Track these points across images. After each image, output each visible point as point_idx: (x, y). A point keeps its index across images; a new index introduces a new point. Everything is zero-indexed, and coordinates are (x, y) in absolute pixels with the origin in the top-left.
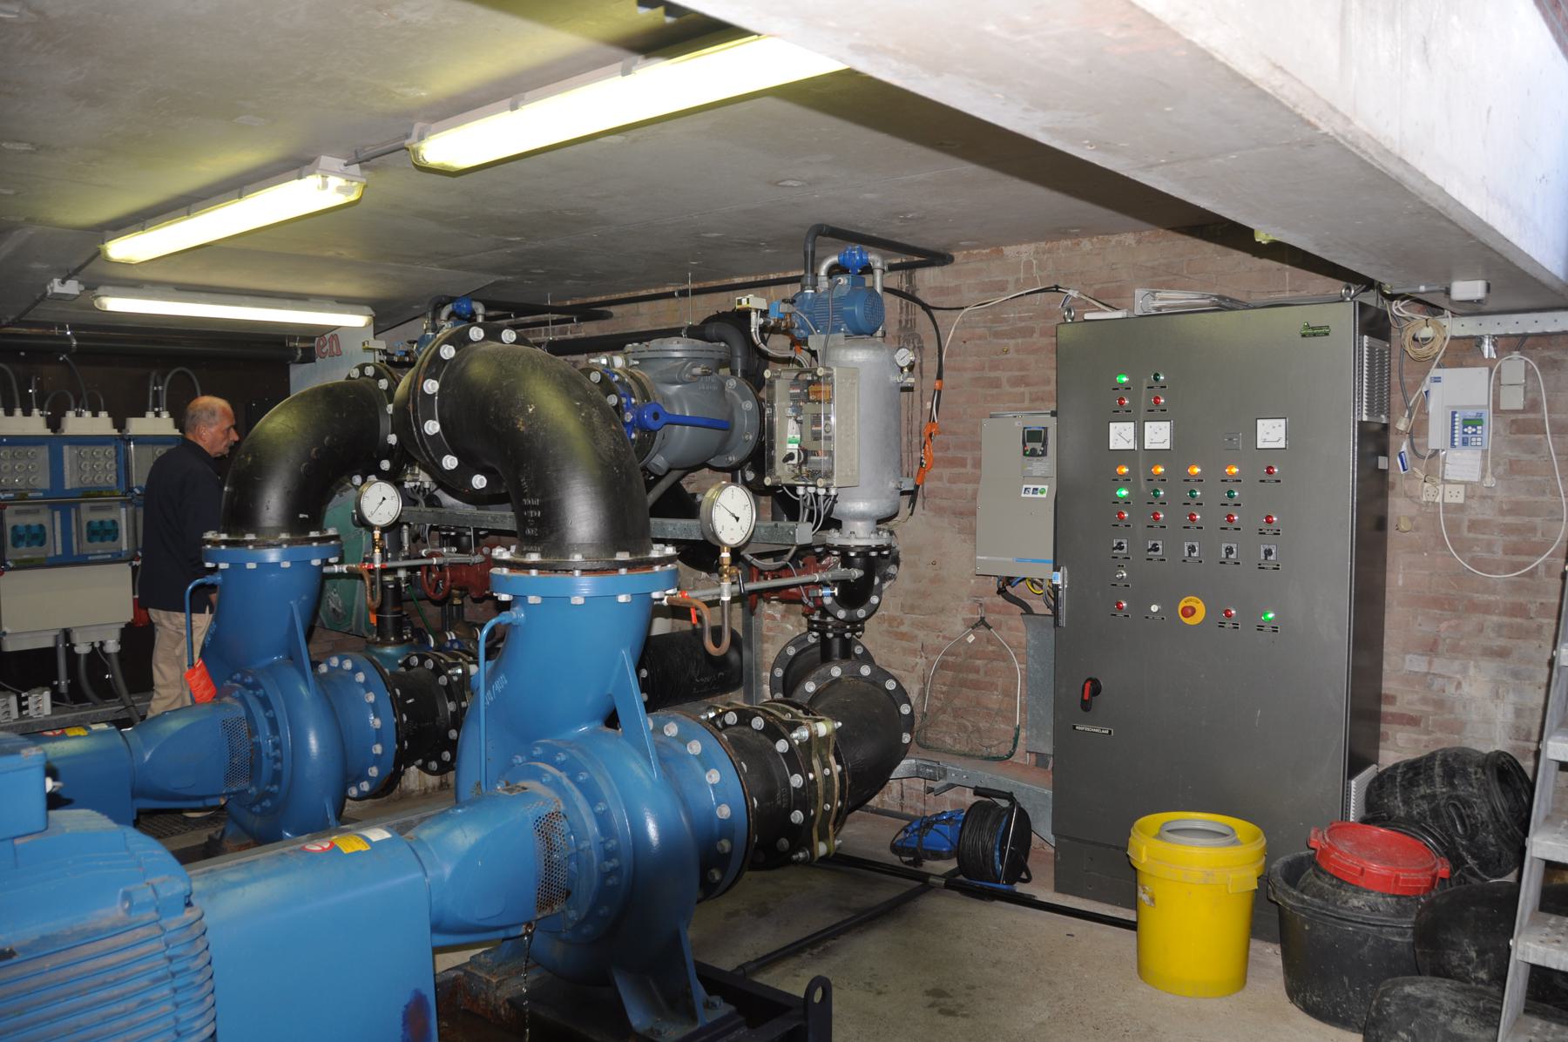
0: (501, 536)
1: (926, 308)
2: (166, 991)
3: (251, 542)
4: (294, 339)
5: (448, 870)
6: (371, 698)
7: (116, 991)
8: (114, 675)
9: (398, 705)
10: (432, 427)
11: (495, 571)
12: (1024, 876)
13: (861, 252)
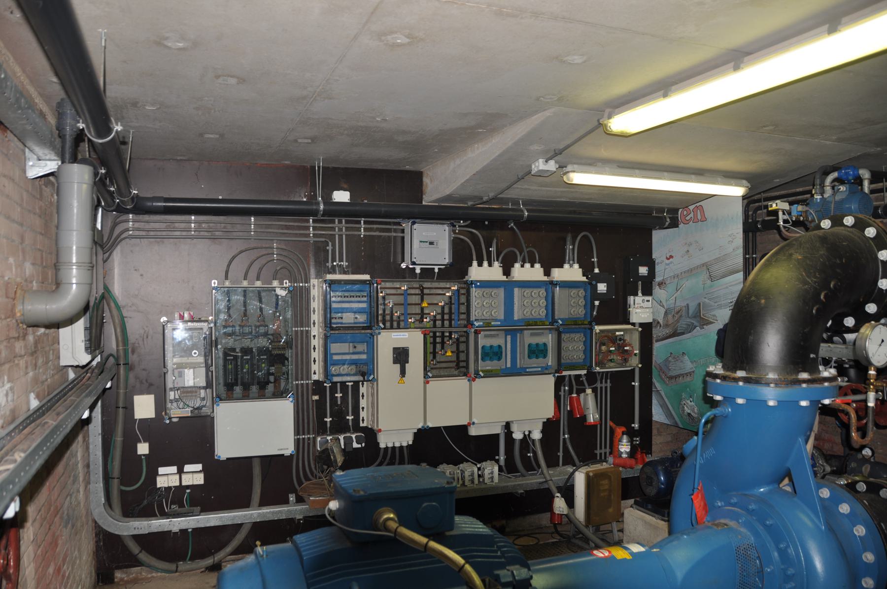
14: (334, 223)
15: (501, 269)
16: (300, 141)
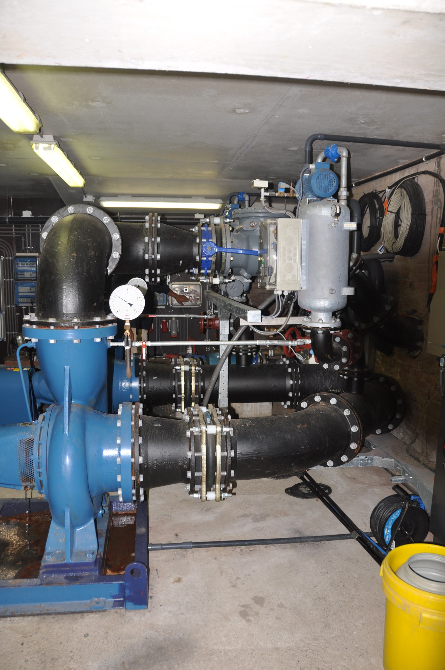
14: (25, 227)
16: (238, 111)
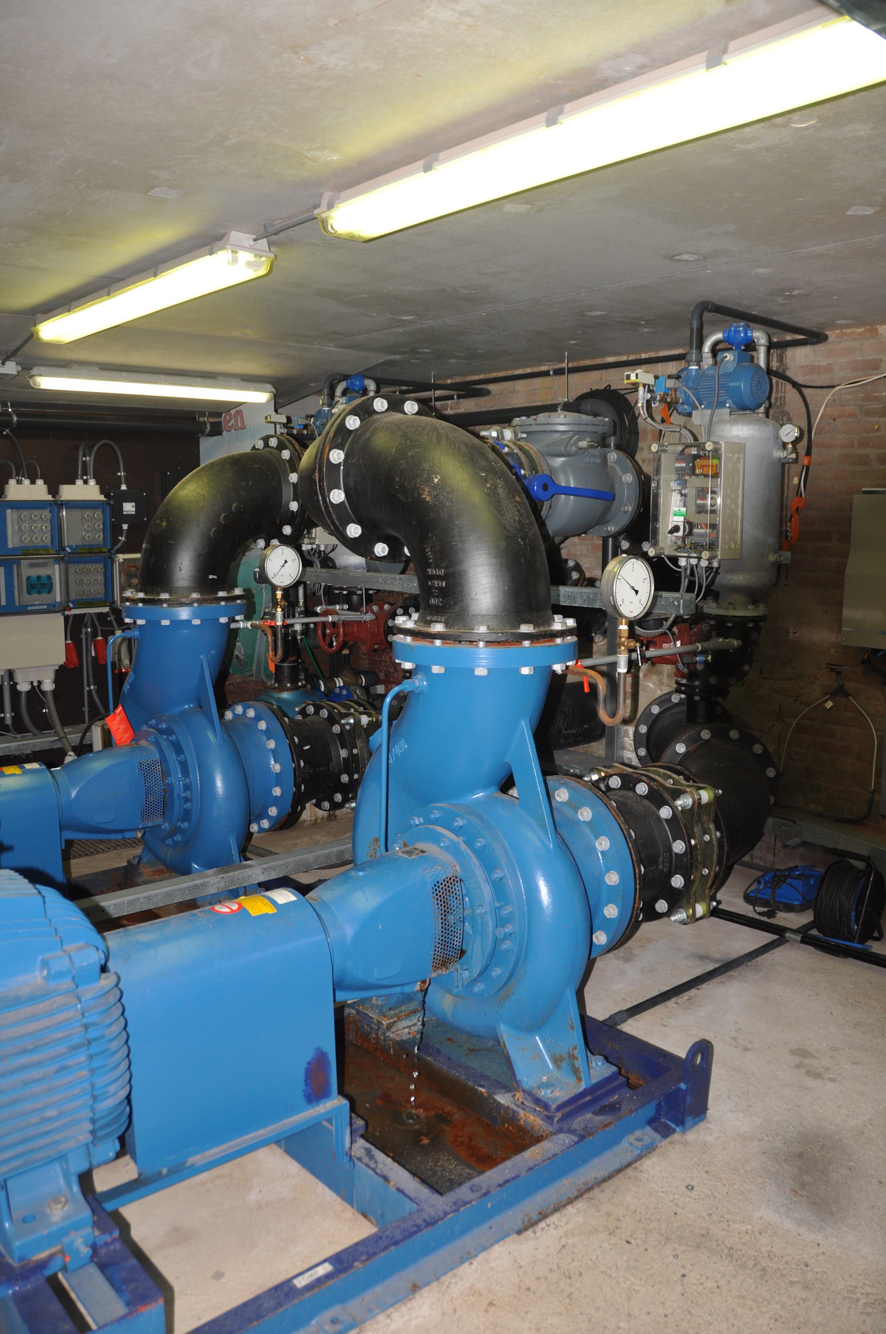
0: (409, 604)
1: (796, 386)
2: (83, 1058)
3: (165, 601)
4: (202, 414)
5: (349, 931)
6: (272, 744)
7: (35, 1057)
8: (50, 709)
9: (296, 752)
10: (337, 496)
11: (399, 638)
12: (876, 934)
13: (747, 328)
15: (97, 487)
